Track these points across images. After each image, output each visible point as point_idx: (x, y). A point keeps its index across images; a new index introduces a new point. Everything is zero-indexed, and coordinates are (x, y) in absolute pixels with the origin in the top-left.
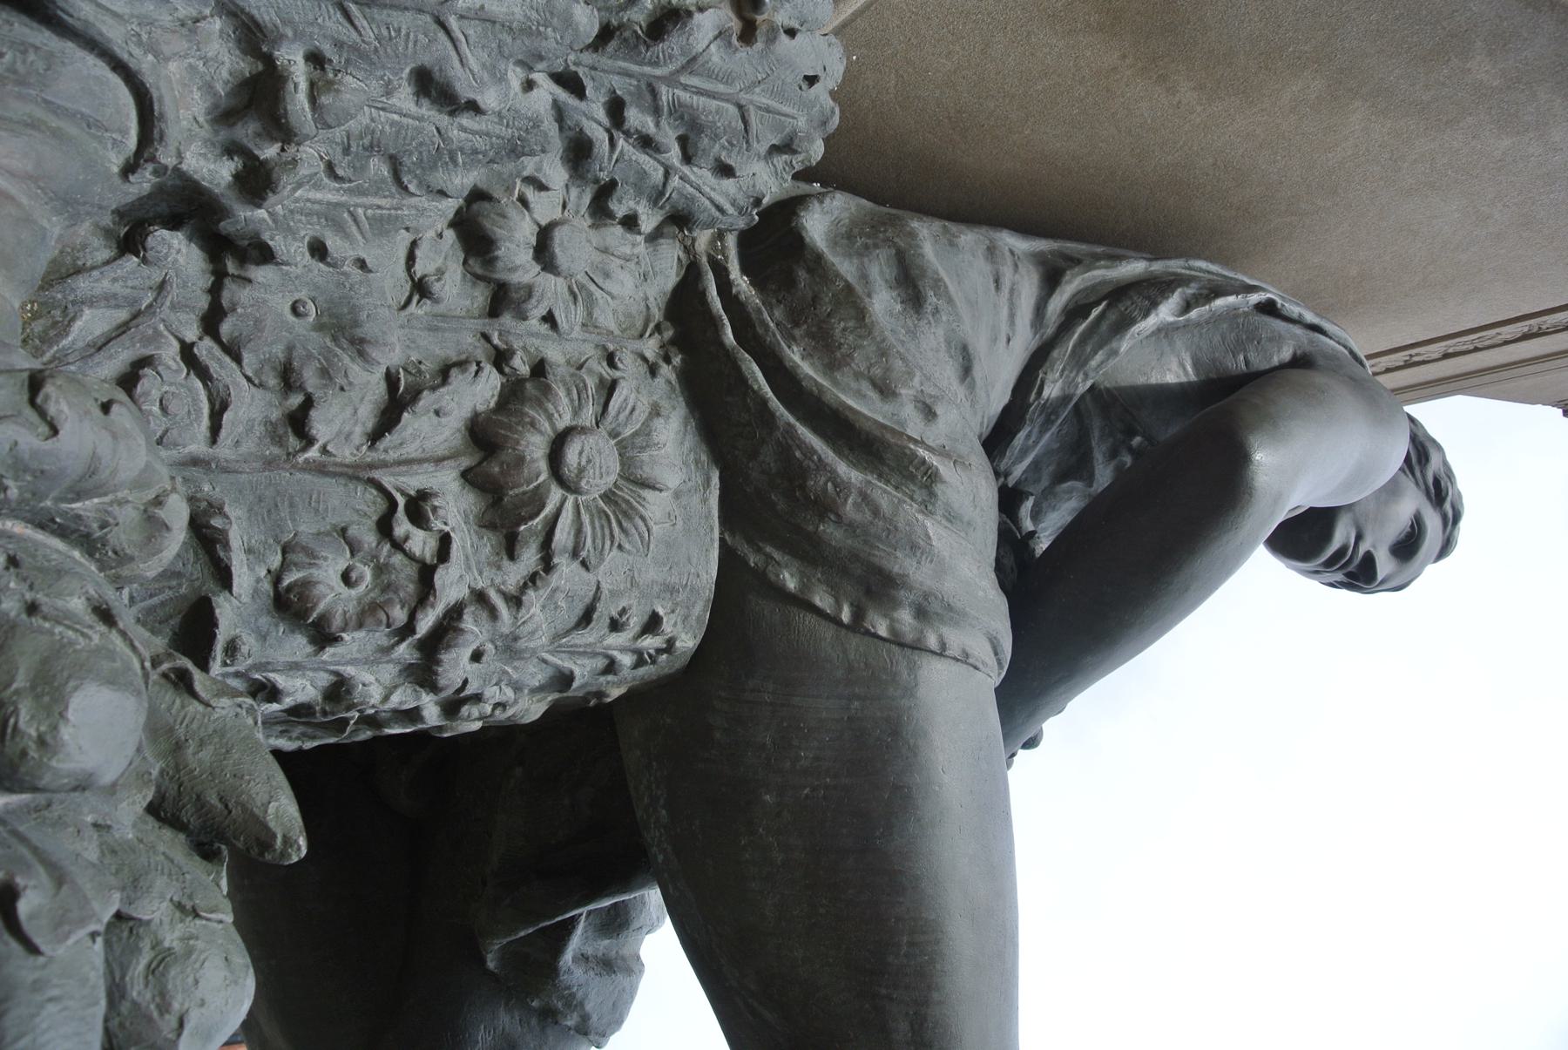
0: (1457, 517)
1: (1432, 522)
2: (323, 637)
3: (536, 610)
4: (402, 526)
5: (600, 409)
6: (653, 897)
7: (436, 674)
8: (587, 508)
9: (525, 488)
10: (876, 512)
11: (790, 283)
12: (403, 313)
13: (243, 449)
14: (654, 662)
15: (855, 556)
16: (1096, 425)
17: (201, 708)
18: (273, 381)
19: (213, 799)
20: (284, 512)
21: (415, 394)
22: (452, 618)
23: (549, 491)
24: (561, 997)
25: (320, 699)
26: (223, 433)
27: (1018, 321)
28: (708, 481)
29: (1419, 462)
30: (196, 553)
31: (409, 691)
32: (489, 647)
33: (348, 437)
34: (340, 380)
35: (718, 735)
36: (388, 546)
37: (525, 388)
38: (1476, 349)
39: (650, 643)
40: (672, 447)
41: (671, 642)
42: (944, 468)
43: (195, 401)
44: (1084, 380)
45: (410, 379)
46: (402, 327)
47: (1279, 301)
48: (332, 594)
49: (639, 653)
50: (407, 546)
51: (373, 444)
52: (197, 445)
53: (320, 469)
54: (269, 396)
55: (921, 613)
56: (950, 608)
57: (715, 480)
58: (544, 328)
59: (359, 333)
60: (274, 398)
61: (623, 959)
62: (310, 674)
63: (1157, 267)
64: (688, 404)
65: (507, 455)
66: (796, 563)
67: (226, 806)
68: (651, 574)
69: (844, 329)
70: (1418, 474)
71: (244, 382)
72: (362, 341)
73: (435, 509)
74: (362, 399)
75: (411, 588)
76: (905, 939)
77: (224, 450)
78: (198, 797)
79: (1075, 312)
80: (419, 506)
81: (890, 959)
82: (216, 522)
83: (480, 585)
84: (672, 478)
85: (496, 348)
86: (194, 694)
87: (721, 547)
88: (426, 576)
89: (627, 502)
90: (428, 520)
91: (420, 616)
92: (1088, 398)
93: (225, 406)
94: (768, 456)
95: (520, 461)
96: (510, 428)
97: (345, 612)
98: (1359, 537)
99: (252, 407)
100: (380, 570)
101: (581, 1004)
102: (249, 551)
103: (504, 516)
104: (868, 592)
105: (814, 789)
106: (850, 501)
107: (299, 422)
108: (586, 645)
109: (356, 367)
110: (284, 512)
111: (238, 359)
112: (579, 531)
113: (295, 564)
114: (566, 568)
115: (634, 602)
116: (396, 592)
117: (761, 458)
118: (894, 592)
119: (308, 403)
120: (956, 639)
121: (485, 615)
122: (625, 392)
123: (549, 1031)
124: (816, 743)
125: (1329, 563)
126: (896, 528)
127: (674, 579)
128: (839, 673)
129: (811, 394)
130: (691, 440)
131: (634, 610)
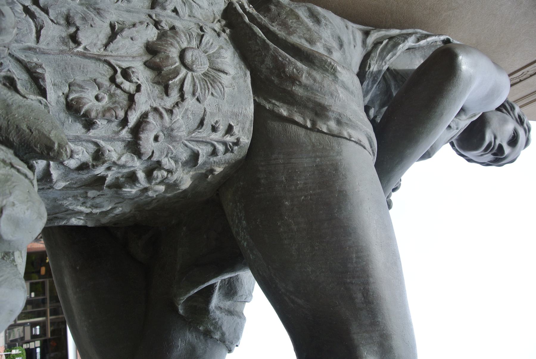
0: (529, 130)
1: (521, 132)
2: (89, 124)
3: (179, 117)
4: (120, 79)
5: (199, 43)
6: (247, 277)
7: (139, 145)
8: (197, 77)
9: (170, 67)
10: (315, 80)
11: (269, 10)
12: (116, 4)
13: (51, 47)
14: (232, 151)
15: (309, 99)
16: (392, 83)
17: (21, 98)
18: (62, 22)
19: (24, 127)
20: (69, 71)
21: (122, 30)
22: (144, 118)
23: (180, 69)
24: (212, 324)
25: (91, 160)
26: (41, 38)
27: (357, 41)
28: (246, 74)
29: (511, 110)
30: (31, 85)
31: (129, 156)
32: (161, 134)
33: (95, 45)
34: (90, 22)
35: (263, 181)
36: (114, 87)
37: (167, 34)
38: (521, 81)
39: (229, 139)
40: (229, 59)
41: (238, 140)
42: (339, 68)
43: (29, 26)
44: (385, 65)
45: (120, 25)
46: (116, 9)
47: (451, 40)
48: (90, 102)
49: (225, 144)
50: (122, 86)
51: (106, 47)
52: (31, 42)
53: (83, 55)
54: (61, 28)
55: (339, 122)
56: (350, 120)
57: (248, 73)
58: (174, 14)
59: (97, 6)
60: (63, 28)
61: (237, 312)
62: (84, 143)
63: (404, 31)
64: (234, 47)
65: (162, 55)
66: (286, 106)
67: (31, 130)
68: (226, 108)
69: (292, 22)
70: (511, 113)
71: (50, 22)
72: (99, 9)
73: (133, 72)
74: (100, 32)
75: (125, 103)
76: (354, 256)
77: (42, 45)
78: (17, 127)
79: (376, 44)
80: (126, 74)
81: (349, 265)
82: (39, 71)
83: (155, 106)
84: (232, 71)
85: (154, 20)
86: (17, 91)
87: (254, 104)
88: (131, 98)
89: (213, 76)
90: (130, 76)
91: (129, 113)
92: (388, 73)
93: (42, 27)
94: (268, 62)
95: (168, 57)
96: (162, 45)
97: (97, 110)
98: (495, 138)
99: (53, 32)
100: (111, 96)
101: (221, 327)
102: (54, 85)
103: (163, 80)
104: (317, 114)
105: (305, 197)
106: (304, 76)
107: (74, 38)
108: (203, 137)
109: (96, 18)
110: (69, 71)
111: (47, 13)
112: (194, 85)
113: (74, 91)
114: (190, 102)
115: (221, 119)
116: (119, 103)
117: (266, 63)
118: (327, 113)
119: (78, 29)
120: (355, 135)
121: (157, 116)
122: (208, 38)
123: (209, 341)
124: (304, 177)
125: (486, 150)
126: (323, 86)
127: (236, 110)
128: (309, 148)
129: (282, 39)
130: (237, 60)
131: (221, 122)
